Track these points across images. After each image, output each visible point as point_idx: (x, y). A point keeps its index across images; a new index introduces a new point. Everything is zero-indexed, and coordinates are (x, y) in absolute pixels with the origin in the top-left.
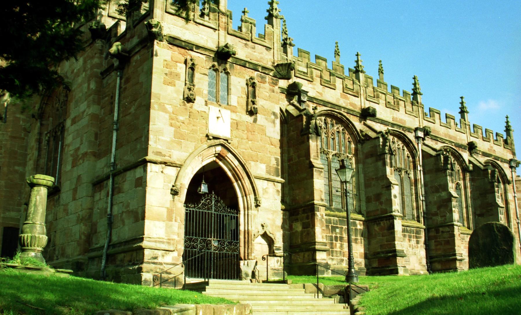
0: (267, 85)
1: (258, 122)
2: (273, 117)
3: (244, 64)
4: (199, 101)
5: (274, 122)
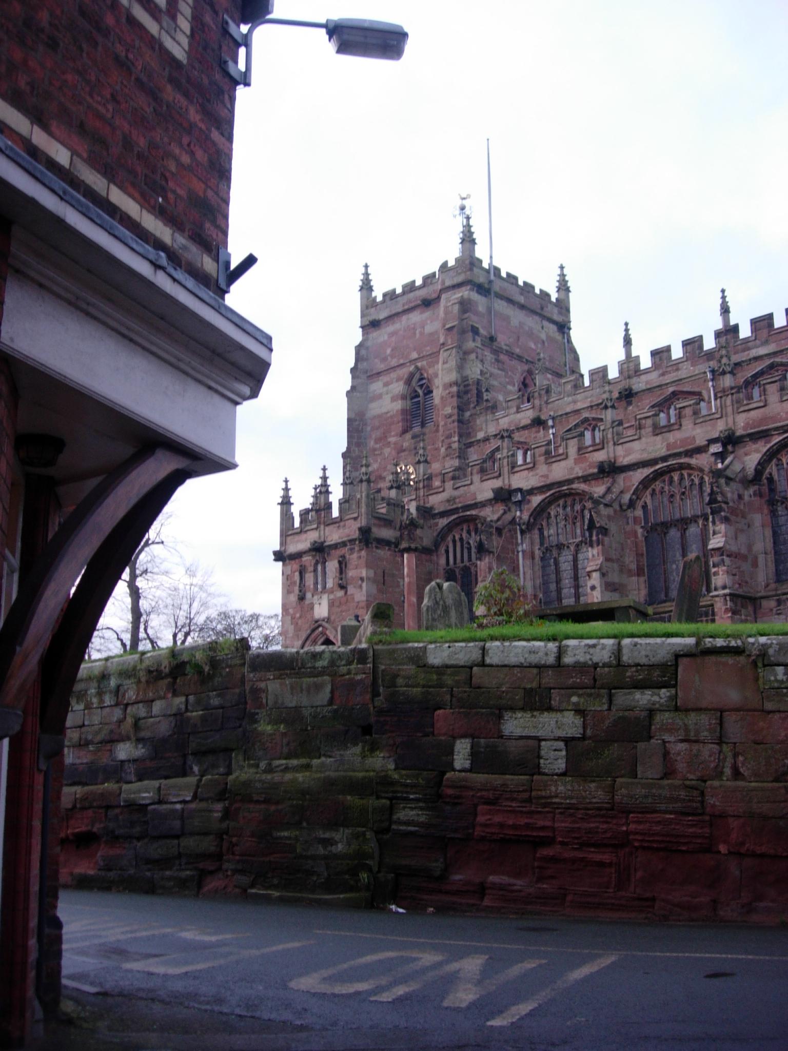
0: (355, 555)
3: (335, 546)
4: (309, 595)
5: (361, 587)
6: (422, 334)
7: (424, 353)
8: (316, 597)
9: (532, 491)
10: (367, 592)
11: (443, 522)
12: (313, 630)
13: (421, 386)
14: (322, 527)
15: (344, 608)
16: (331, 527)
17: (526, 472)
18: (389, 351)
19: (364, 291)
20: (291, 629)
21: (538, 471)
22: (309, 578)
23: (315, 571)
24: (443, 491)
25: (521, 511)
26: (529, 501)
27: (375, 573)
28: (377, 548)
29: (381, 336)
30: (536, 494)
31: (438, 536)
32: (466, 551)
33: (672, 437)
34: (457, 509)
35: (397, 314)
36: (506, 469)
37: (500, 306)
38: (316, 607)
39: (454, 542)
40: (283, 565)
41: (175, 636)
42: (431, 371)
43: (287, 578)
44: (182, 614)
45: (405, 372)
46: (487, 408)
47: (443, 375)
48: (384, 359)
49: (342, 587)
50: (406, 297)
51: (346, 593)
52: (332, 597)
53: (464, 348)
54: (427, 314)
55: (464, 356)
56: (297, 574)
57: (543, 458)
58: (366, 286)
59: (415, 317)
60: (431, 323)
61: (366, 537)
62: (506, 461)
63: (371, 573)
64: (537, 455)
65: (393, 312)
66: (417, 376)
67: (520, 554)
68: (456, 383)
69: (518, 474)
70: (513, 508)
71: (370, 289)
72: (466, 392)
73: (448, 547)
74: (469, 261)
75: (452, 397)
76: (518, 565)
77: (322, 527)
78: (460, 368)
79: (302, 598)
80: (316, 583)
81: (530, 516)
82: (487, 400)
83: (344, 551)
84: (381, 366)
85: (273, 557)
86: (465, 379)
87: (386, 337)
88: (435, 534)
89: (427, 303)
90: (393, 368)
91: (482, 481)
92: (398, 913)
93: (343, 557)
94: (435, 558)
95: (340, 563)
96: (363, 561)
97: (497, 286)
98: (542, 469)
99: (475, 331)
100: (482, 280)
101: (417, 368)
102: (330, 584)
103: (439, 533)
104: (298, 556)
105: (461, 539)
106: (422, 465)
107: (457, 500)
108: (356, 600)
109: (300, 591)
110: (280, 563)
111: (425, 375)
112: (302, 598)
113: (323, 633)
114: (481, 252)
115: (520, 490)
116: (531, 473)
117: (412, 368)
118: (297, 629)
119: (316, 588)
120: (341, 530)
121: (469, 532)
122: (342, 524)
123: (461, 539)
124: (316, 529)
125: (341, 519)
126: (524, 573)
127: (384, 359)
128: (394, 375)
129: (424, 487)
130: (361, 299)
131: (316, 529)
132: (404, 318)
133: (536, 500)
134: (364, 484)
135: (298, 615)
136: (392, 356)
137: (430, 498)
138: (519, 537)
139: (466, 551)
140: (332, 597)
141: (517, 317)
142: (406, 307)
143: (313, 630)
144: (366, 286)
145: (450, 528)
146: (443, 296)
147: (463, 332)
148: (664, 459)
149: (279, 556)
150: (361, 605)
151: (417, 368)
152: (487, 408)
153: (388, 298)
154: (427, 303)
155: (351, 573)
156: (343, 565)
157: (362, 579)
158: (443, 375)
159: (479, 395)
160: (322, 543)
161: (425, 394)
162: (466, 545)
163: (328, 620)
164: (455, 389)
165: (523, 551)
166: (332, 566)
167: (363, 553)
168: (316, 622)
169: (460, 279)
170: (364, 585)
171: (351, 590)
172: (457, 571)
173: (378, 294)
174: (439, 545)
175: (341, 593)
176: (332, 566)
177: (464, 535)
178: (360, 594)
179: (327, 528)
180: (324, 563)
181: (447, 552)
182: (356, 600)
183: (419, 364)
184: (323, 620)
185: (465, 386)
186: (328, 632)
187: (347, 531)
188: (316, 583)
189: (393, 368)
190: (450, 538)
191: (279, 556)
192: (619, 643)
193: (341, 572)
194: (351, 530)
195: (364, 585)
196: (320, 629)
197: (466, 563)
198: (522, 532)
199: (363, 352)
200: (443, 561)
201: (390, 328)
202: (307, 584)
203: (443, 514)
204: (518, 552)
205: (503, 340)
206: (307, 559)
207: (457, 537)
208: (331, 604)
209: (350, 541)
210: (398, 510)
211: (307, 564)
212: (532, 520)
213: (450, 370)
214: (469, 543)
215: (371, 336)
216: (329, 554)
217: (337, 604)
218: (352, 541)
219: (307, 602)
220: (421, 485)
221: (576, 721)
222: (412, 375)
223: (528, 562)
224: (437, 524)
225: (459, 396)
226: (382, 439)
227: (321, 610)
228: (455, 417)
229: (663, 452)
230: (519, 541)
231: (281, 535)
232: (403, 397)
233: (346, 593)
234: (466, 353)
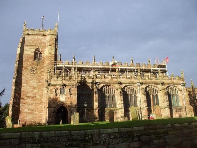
13: (39, 52)
18: (31, 42)
33: (130, 80)
36: (95, 78)
48: (30, 43)
51: (71, 96)
59: (39, 37)
84: (29, 44)
87: (31, 38)
92: (177, 124)
98: (103, 79)
117: (38, 47)
127: (30, 43)
133: (102, 85)
148: (128, 84)
192: (71, 132)
208: (66, 98)
221: (167, 113)
222: (37, 49)
226: (28, 60)
229: (128, 82)
233: (71, 96)
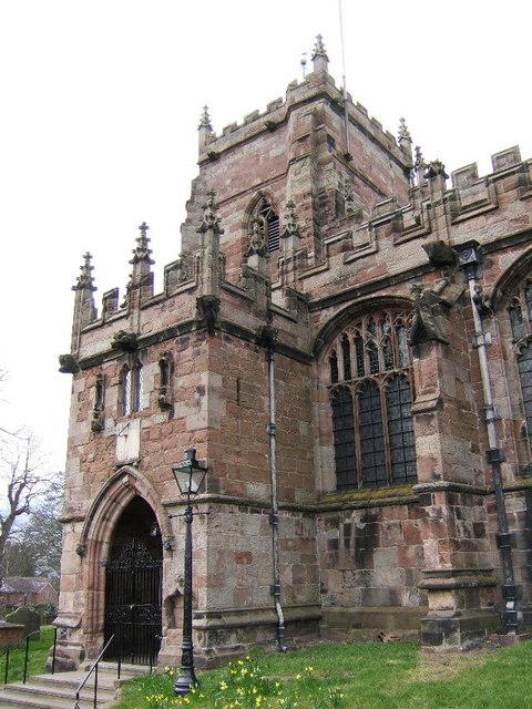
0: (189, 351)
1: (176, 417)
2: (197, 395)
3: (156, 339)
4: (109, 423)
5: (198, 404)
6: (266, 159)
7: (269, 177)
8: (120, 425)
9: (497, 246)
10: (210, 411)
11: (327, 314)
12: (114, 481)
14: (136, 311)
15: (167, 442)
16: (151, 310)
17: (482, 218)
18: (228, 182)
19: (203, 130)
20: (79, 478)
21: (506, 214)
22: (112, 395)
23: (122, 383)
24: (328, 269)
25: (476, 279)
26: (492, 263)
27: (224, 380)
28: (227, 339)
29: (221, 169)
30: (504, 250)
31: (319, 336)
32: (366, 359)
34: (354, 291)
35: (239, 145)
37: (353, 130)
38: (120, 441)
39: (346, 345)
40: (75, 378)
41: (11, 487)
42: (276, 195)
43: (79, 396)
44: (21, 467)
45: (246, 200)
46: (351, 218)
47: (293, 190)
49: (166, 406)
50: (247, 127)
52: (146, 423)
53: (320, 158)
54: (272, 139)
55: (319, 168)
56: (94, 389)
57: (514, 193)
58: (206, 125)
59: (259, 144)
60: (278, 147)
61: (208, 319)
62: (439, 210)
63: (218, 381)
64: (501, 189)
65: (234, 143)
66: (260, 203)
67: (482, 350)
68: (310, 194)
69: (466, 223)
70: (461, 277)
71: (210, 128)
72: (323, 205)
73: (334, 353)
74: (324, 79)
75: (307, 208)
76: (479, 368)
77: (136, 311)
78: (316, 178)
79: (98, 429)
80: (122, 403)
81: (497, 286)
82: (350, 210)
83: (171, 345)
85: (59, 366)
86: (321, 191)
88: (315, 333)
89: (272, 128)
90: (233, 198)
91: (396, 245)
93: (169, 354)
94: (314, 370)
95: (163, 365)
96: (204, 358)
97: (350, 110)
99: (331, 141)
100: (334, 96)
101: (260, 194)
102: (144, 401)
103: (322, 332)
104: (98, 360)
105: (358, 340)
106: (291, 238)
107: (351, 280)
108: (189, 427)
109: (96, 417)
110: (70, 376)
111: (270, 201)
112: (98, 429)
113: (129, 487)
114: (333, 70)
115: (473, 244)
116: (492, 219)
117: (255, 194)
118: (89, 480)
119: (122, 411)
120: (166, 313)
121: (369, 328)
122: (168, 302)
123: (358, 340)
124: (126, 317)
125: (168, 295)
126: (492, 384)
128: (232, 205)
129: (295, 269)
130: (200, 136)
131: (126, 317)
132: (246, 148)
134: (209, 233)
135: (91, 456)
136: (231, 186)
137: (305, 282)
138: (477, 321)
139: (366, 359)
140: (146, 423)
141: (370, 148)
142: (248, 135)
143: (114, 481)
144: (206, 125)
145: (338, 323)
146: (292, 119)
147: (317, 143)
149: (69, 365)
150: (198, 435)
151: (260, 194)
152: (351, 218)
153: (228, 132)
154: (272, 128)
155: (181, 382)
156: (167, 367)
157: (200, 390)
158: (293, 190)
159: (339, 207)
160: (134, 336)
161: (269, 221)
162: (366, 348)
163: (138, 464)
164: (310, 199)
165: (487, 346)
166: (150, 372)
167: (205, 346)
168: (119, 467)
169: (313, 92)
170: (205, 400)
171: (180, 409)
172: (352, 388)
173: (218, 131)
174: (321, 350)
175: (161, 417)
176: (150, 372)
177: (363, 332)
178: (195, 417)
179: (143, 313)
180: (137, 368)
181: (333, 361)
182: (189, 427)
183: (263, 189)
184: (130, 464)
185: (320, 199)
186: (137, 485)
187: (176, 312)
188: (122, 403)
189: (233, 198)
190: (338, 341)
191: (69, 365)
193: (164, 381)
194: (186, 308)
195: (205, 400)
196: (126, 479)
197: (368, 375)
198: (484, 313)
199: (200, 186)
200: (326, 375)
201: (231, 159)
202: (107, 405)
203: (326, 303)
204: (476, 347)
205: (356, 163)
206: (111, 368)
207: (351, 337)
208: (145, 438)
209: (181, 327)
210: (262, 288)
211: (110, 373)
212: (499, 293)
213: (302, 181)
214: (371, 345)
215: (208, 171)
216: (145, 353)
217: (154, 435)
218: (184, 328)
219: (106, 434)
220: (290, 266)
222: (254, 203)
223: (499, 364)
224: (316, 319)
225: (314, 208)
227: (128, 447)
228: (311, 230)
230: (478, 329)
231: (74, 334)
232: (244, 226)
234: (321, 164)
